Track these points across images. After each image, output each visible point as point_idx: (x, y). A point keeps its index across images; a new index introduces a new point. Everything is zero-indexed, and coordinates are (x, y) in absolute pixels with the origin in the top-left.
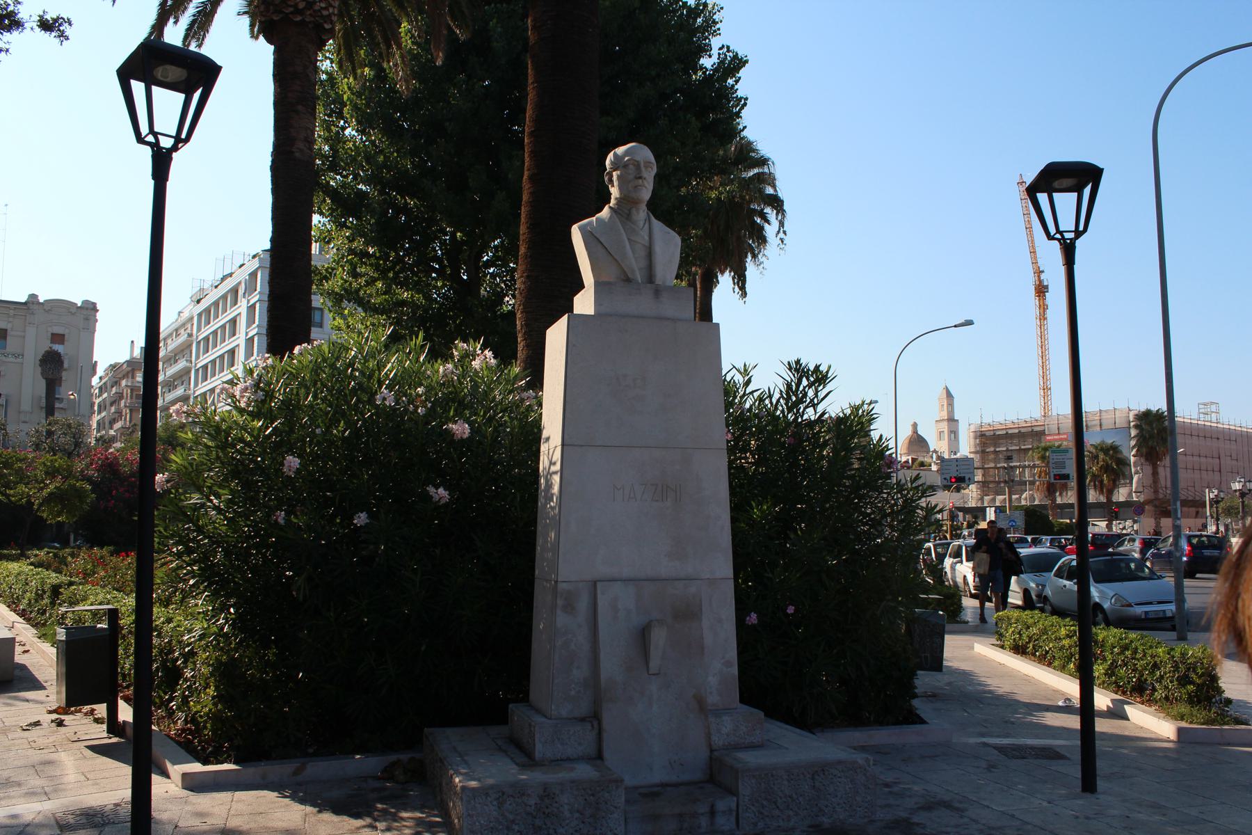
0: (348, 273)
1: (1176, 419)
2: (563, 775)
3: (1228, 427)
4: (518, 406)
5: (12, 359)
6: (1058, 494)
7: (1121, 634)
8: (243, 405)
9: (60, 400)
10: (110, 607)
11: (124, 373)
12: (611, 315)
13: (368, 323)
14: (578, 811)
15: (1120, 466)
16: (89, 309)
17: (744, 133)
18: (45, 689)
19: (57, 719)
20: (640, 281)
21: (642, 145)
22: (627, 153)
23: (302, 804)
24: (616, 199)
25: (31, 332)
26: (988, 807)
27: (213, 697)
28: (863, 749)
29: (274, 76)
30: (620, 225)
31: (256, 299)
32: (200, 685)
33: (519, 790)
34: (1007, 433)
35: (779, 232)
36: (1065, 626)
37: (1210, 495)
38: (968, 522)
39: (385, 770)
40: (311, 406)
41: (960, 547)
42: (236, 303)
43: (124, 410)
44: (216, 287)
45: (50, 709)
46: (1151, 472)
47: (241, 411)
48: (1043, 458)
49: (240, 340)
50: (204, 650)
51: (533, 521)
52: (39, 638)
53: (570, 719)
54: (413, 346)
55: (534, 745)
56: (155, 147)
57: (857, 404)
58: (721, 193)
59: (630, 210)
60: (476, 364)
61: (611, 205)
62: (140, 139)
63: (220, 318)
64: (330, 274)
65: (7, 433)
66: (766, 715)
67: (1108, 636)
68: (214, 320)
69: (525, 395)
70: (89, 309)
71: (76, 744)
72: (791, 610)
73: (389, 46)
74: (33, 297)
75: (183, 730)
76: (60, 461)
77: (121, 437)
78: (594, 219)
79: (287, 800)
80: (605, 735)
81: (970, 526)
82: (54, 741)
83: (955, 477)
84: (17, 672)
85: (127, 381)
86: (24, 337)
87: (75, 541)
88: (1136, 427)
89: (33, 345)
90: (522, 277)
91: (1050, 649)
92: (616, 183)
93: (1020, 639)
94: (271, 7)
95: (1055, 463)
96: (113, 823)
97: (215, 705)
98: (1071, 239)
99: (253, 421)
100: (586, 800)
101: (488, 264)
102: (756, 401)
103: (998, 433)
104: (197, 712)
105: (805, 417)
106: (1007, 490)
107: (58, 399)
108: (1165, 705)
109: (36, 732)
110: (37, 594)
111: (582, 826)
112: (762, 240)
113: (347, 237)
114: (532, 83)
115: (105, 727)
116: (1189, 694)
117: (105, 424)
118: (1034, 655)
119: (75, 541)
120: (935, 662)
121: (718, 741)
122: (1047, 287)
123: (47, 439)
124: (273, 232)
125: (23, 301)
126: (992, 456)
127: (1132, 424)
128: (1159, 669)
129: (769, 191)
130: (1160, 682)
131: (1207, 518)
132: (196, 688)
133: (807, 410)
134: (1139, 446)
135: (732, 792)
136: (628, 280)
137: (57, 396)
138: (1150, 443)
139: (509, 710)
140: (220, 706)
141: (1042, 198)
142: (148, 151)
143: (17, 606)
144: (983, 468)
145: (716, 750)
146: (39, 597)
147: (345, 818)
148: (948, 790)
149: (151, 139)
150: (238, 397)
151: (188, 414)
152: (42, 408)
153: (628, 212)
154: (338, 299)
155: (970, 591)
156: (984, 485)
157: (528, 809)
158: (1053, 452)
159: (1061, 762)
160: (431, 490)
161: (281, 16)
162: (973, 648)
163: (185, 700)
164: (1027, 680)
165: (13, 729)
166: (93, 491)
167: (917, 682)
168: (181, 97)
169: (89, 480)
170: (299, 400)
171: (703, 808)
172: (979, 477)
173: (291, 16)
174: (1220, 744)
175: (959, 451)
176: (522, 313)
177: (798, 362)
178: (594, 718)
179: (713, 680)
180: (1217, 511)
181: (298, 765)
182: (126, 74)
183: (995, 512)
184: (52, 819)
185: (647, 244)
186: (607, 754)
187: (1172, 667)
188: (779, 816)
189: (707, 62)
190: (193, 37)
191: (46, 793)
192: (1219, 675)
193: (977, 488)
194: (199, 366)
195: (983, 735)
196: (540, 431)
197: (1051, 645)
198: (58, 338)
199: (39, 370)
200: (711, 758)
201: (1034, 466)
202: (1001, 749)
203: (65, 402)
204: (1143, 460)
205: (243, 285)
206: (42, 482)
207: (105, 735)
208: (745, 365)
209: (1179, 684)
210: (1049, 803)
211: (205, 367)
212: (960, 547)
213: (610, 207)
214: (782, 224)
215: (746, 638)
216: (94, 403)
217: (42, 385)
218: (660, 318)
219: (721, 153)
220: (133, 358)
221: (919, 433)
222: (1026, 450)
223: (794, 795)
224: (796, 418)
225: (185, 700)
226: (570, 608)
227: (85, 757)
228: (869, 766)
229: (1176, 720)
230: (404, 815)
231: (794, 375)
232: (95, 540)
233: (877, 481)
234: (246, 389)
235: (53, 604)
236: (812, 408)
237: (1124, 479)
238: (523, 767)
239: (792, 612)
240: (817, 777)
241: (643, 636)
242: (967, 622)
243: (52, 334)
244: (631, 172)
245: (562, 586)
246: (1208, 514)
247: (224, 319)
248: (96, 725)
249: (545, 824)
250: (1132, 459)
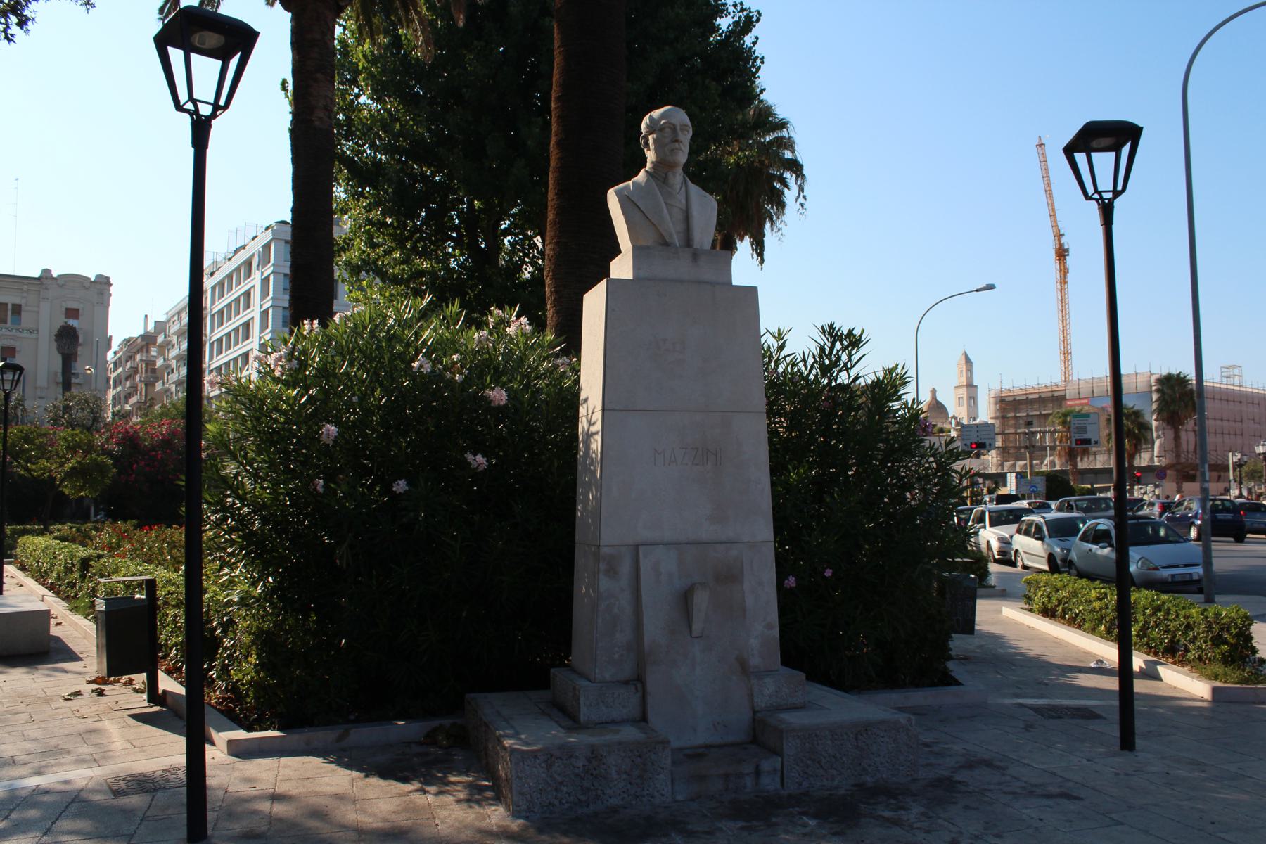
0: (365, 243)
1: (1205, 384)
2: (609, 737)
3: (1250, 390)
4: (551, 373)
5: (25, 334)
6: (1079, 459)
7: (1153, 596)
8: (277, 374)
9: (77, 375)
10: (148, 577)
11: (138, 347)
13: (387, 294)
14: (626, 772)
15: (1143, 431)
16: (103, 285)
17: (763, 97)
18: (82, 660)
19: (97, 689)
21: (677, 108)
22: (663, 116)
23: (348, 769)
24: (652, 162)
25: (45, 308)
26: (1028, 765)
27: (256, 665)
28: (900, 709)
29: (292, 43)
30: (656, 188)
31: (270, 270)
32: (241, 653)
33: (567, 752)
34: (1027, 398)
35: (798, 197)
36: (1095, 588)
37: (1233, 459)
38: (988, 488)
39: (428, 736)
40: (347, 373)
41: (983, 513)
42: (249, 276)
43: (139, 385)
44: (229, 259)
45: (88, 679)
46: (1173, 436)
47: (276, 380)
48: (1064, 423)
49: (254, 313)
50: (245, 619)
51: (572, 486)
52: (71, 610)
53: (613, 682)
54: (448, 313)
55: (579, 708)
56: (194, 113)
57: (890, 367)
58: (740, 158)
59: (666, 174)
60: (511, 331)
61: (647, 168)
62: (179, 107)
63: (234, 290)
64: (348, 244)
65: (25, 410)
66: (808, 678)
67: (1139, 598)
68: (228, 293)
69: (559, 361)
71: (118, 713)
72: (828, 573)
73: (407, 11)
74: (46, 272)
75: (224, 699)
76: (80, 436)
77: (136, 412)
78: (630, 183)
79: (333, 766)
80: (650, 700)
81: (990, 492)
82: (97, 711)
83: (975, 443)
84: (52, 644)
85: (142, 356)
86: (38, 312)
87: (96, 515)
88: (1158, 391)
89: (48, 320)
90: (551, 243)
91: (1080, 611)
92: (652, 147)
93: (1049, 602)
95: (1077, 428)
96: (164, 788)
97: (257, 672)
98: (1109, 199)
99: (288, 389)
100: (633, 761)
101: (507, 232)
102: (788, 365)
103: (1018, 398)
104: (238, 681)
105: (839, 381)
106: (1028, 455)
107: (74, 374)
108: (1199, 665)
109: (76, 703)
110: (66, 567)
112: (781, 205)
113: (365, 208)
114: (559, 47)
115: (145, 696)
116: (1223, 654)
117: (120, 398)
118: (1064, 618)
119: (96, 515)
120: (968, 625)
121: (761, 702)
122: (1067, 250)
123: (64, 414)
126: (1012, 422)
127: (1154, 388)
128: (1192, 629)
129: (788, 155)
130: (1193, 642)
131: (1230, 482)
132: (237, 657)
133: (841, 374)
134: (1160, 411)
135: (777, 752)
136: (665, 244)
137: (73, 371)
138: (1172, 408)
139: (551, 675)
140: (262, 674)
141: (1080, 158)
142: (186, 119)
143: (45, 580)
144: (1003, 433)
145: (758, 712)
146: (69, 570)
147: (392, 782)
148: (987, 749)
149: (190, 106)
150: (272, 367)
151: (222, 384)
152: (58, 383)
153: (664, 175)
154: (355, 269)
155: (993, 556)
156: (1005, 452)
157: (577, 771)
158: (1075, 417)
159: (1097, 721)
160: (469, 456)
162: (1001, 612)
163: (225, 670)
164: (1058, 642)
165: (55, 698)
166: (114, 465)
167: (951, 644)
168: (218, 64)
169: (109, 454)
170: (335, 368)
171: (748, 768)
172: (999, 443)
174: (1254, 703)
175: (978, 417)
176: (551, 279)
177: (831, 326)
178: (638, 680)
179: (754, 643)
180: (1240, 475)
182: (162, 42)
183: (1016, 477)
184: (105, 784)
185: (684, 208)
187: (1206, 627)
189: (724, 23)
191: (95, 760)
192: (1253, 635)
193: (997, 454)
194: (213, 339)
195: (1018, 696)
196: (577, 395)
197: (1081, 608)
198: (72, 313)
199: (55, 345)
200: (754, 720)
201: (1055, 431)
202: (1036, 709)
203: (81, 377)
204: (1164, 425)
206: (64, 456)
207: (146, 704)
208: (779, 330)
209: (1213, 644)
210: (1089, 760)
211: (220, 340)
212: (983, 513)
213: (646, 171)
214: (801, 189)
215: (786, 599)
216: (110, 378)
217: (58, 361)
218: (700, 282)
219: (740, 117)
220: (146, 332)
221: (938, 399)
222: (1047, 415)
224: (830, 382)
225: (225, 670)
226: (612, 572)
227: (129, 726)
228: (911, 725)
229: (1210, 679)
230: (452, 779)
231: (827, 339)
232: (115, 515)
233: (911, 444)
234: (280, 359)
235: (83, 577)
236: (845, 372)
237: (1145, 444)
238: (569, 729)
239: (830, 575)
240: (860, 737)
241: (686, 598)
242: (994, 587)
244: (666, 135)
245: (604, 550)
246: (1231, 477)
247: (238, 292)
248: (136, 695)
249: (593, 786)
250: (1154, 424)
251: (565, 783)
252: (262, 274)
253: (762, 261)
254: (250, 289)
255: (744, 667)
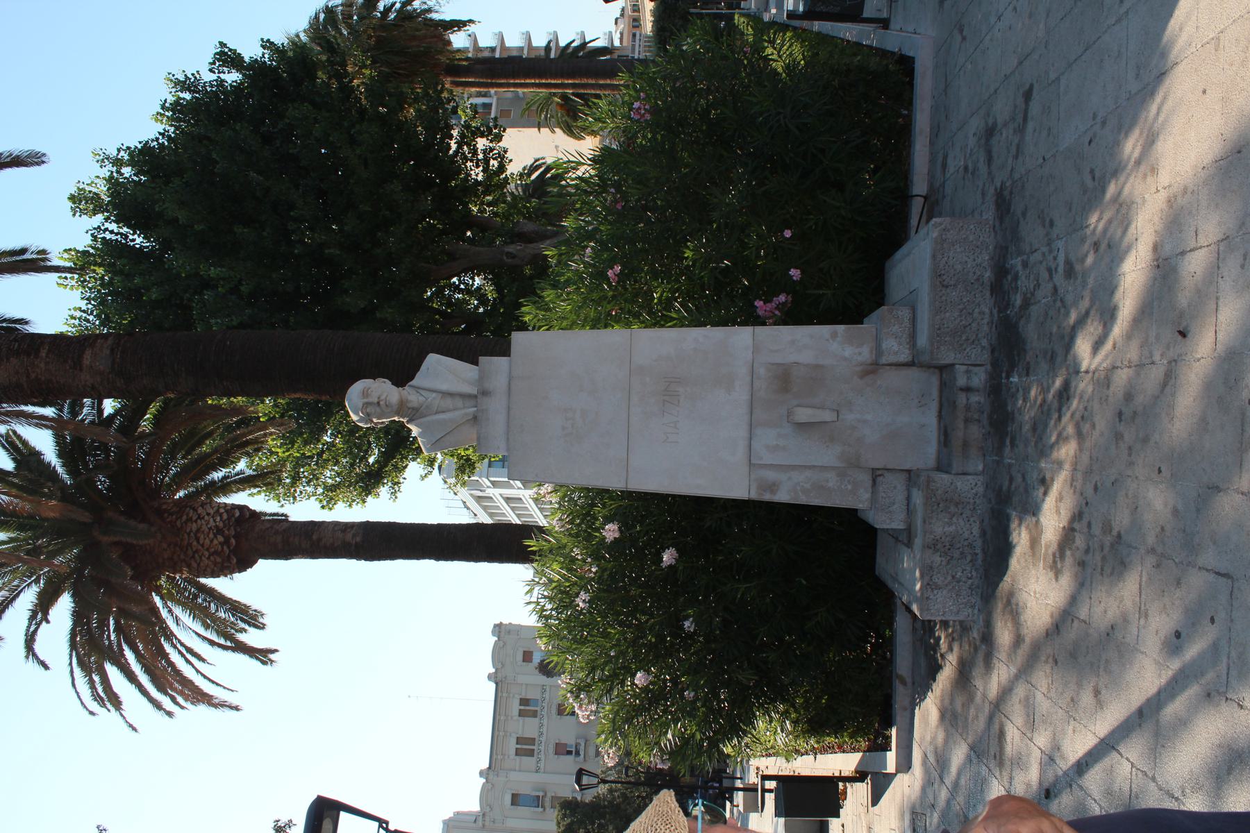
5: (547, 695)
12: (508, 439)
14: (951, 519)
16: (499, 629)
20: (475, 409)
25: (522, 679)
29: (287, 559)
44: (475, 515)
59: (409, 408)
70: (499, 629)
74: (490, 677)
86: (527, 685)
94: (226, 564)
111: (964, 516)
124: (430, 558)
125: (494, 685)
136: (475, 418)
157: (944, 563)
161: (232, 557)
173: (232, 548)
179: (848, 351)
181: (897, 681)
185: (441, 395)
186: (907, 467)
188: (978, 324)
190: (256, 620)
205: (473, 492)
223: (961, 307)
240: (945, 283)
243: (524, 661)
244: (373, 411)
251: (954, 574)
252: (488, 487)
253: (471, 21)
254: (503, 498)
255: (873, 368)
